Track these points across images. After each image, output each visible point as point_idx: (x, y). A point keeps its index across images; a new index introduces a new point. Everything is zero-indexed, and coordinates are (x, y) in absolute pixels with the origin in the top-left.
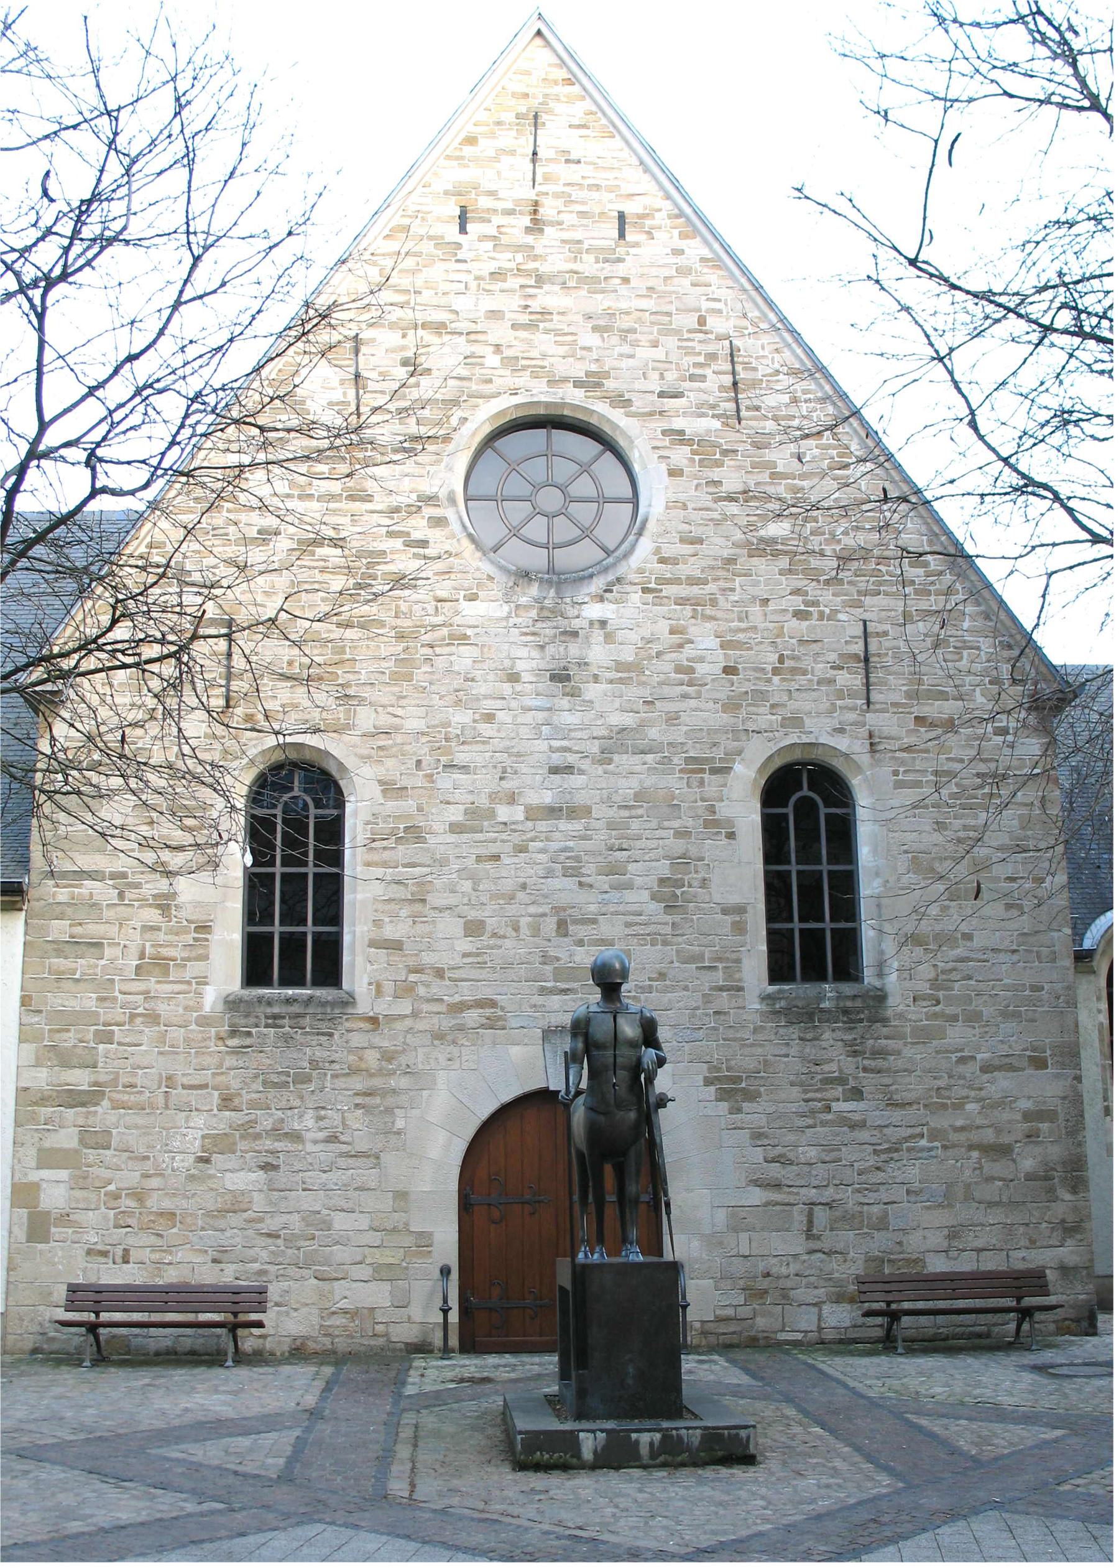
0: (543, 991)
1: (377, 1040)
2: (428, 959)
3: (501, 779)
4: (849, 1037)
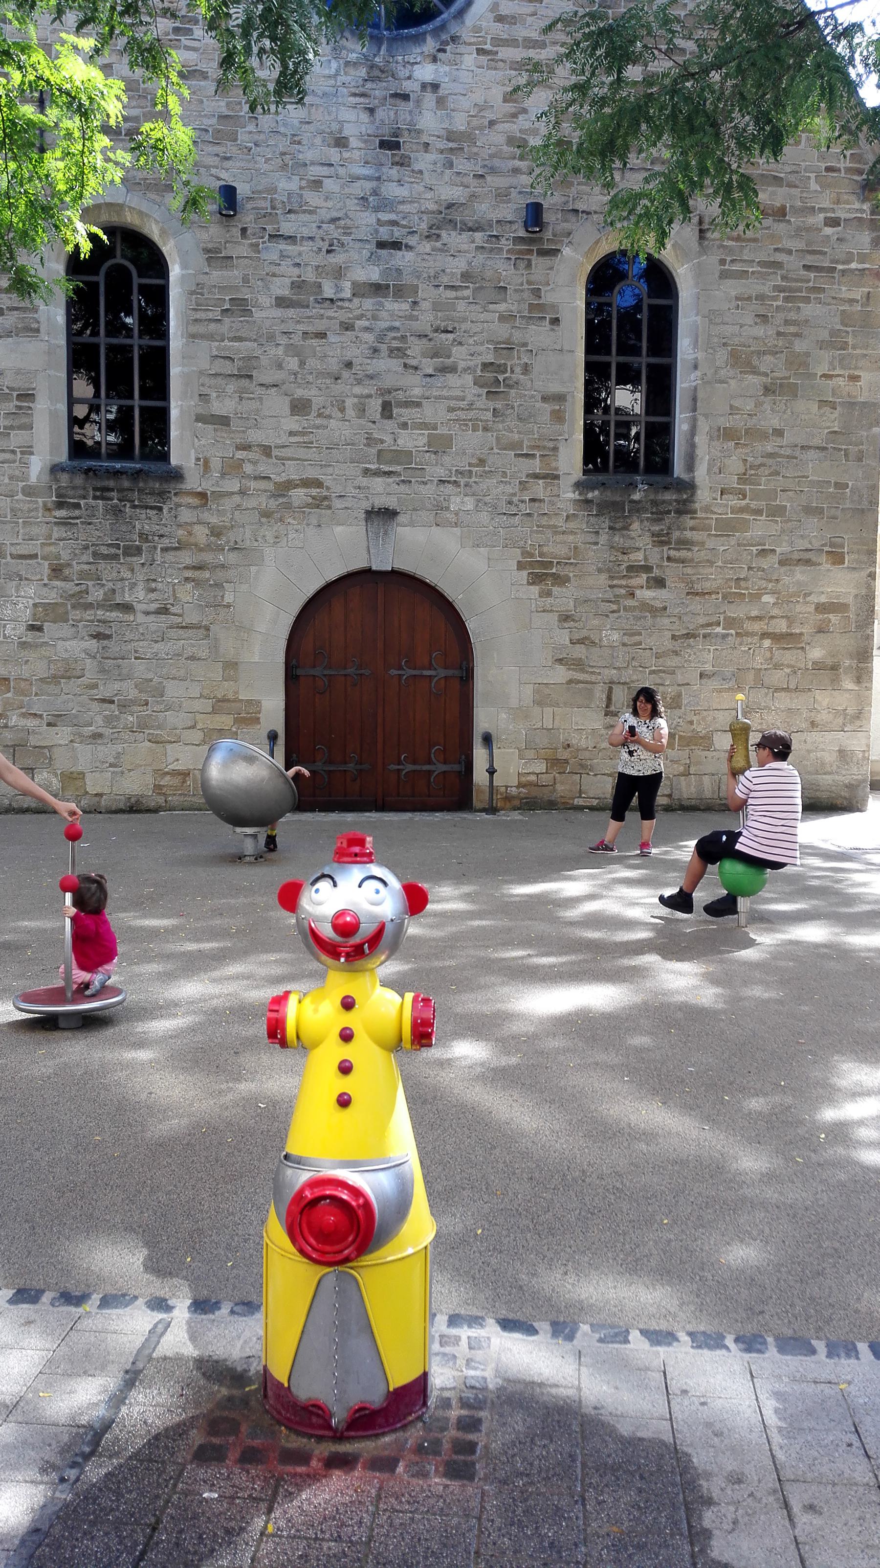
0: (366, 472)
1: (206, 516)
2: (255, 436)
3: (328, 252)
4: (656, 528)
